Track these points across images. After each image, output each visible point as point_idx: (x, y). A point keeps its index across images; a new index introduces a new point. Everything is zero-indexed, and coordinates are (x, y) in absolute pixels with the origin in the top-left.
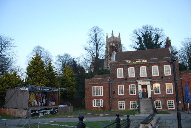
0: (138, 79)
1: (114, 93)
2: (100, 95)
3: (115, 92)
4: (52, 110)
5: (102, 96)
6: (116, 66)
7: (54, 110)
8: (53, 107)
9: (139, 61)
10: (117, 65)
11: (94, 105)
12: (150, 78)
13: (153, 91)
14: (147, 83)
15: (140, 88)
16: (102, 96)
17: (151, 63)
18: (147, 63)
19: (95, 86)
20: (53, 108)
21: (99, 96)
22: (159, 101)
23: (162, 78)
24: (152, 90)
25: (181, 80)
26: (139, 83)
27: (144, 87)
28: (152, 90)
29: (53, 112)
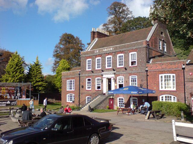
1: (83, 87)
2: (163, 75)
4: (8, 102)
5: (160, 75)
7: (10, 103)
8: (9, 100)
9: (106, 50)
10: (87, 55)
11: (162, 88)
13: (117, 86)
14: (111, 76)
16: (160, 75)
17: (117, 50)
18: (114, 51)
19: (69, 79)
20: (10, 101)
21: (165, 75)
22: (171, 96)
23: (126, 69)
24: (116, 85)
25: (147, 71)
27: (109, 80)
28: (116, 85)
29: (10, 104)
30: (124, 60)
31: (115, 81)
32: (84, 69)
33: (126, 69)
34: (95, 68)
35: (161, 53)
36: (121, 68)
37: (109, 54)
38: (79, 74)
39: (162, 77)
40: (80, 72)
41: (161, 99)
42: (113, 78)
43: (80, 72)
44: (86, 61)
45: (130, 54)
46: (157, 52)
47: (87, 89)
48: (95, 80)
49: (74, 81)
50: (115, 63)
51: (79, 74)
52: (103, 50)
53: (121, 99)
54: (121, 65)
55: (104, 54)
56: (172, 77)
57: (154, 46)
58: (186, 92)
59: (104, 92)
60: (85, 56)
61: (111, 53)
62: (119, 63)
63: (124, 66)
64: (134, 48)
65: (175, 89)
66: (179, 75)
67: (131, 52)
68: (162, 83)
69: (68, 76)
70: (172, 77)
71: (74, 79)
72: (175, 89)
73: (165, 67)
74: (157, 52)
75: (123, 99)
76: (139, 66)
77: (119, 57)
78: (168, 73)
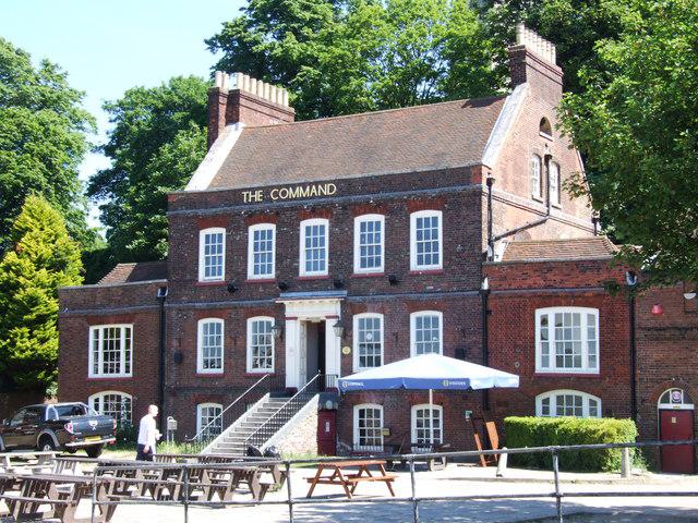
0: (284, 288)
1: (180, 358)
3: (185, 357)
5: (539, 313)
6: (196, 216)
10: (200, 212)
12: (338, 285)
13: (351, 355)
15: (295, 337)
24: (347, 350)
26: (289, 312)
27: (316, 331)
28: (347, 350)
30: (386, 244)
31: (346, 338)
32: (188, 277)
33: (393, 281)
34: (245, 270)
35: (536, 212)
36: (372, 277)
37: (315, 212)
38: (162, 300)
39: (97, 332)
40: (163, 290)
41: (555, 411)
42: (334, 321)
43: (163, 290)
44: (197, 236)
45: (414, 217)
46: (524, 209)
47: (201, 369)
48: (245, 328)
49: (128, 330)
50: (341, 249)
51: (162, 300)
52: (284, 193)
53: (370, 411)
54: (371, 265)
55: (292, 209)
56: (123, 333)
57: (510, 186)
58: (637, 379)
59: (289, 384)
60: (190, 212)
61: (323, 207)
62: (207, 263)
63: (386, 268)
64: (432, 193)
65: (596, 370)
66: (611, 313)
67: (256, 223)
68: (97, 349)
69: (94, 307)
70: (123, 333)
71: (129, 322)
72: (596, 370)
73: (558, 278)
74: (524, 209)
75: (377, 412)
76: (453, 273)
77: (256, 238)
78: (568, 304)
